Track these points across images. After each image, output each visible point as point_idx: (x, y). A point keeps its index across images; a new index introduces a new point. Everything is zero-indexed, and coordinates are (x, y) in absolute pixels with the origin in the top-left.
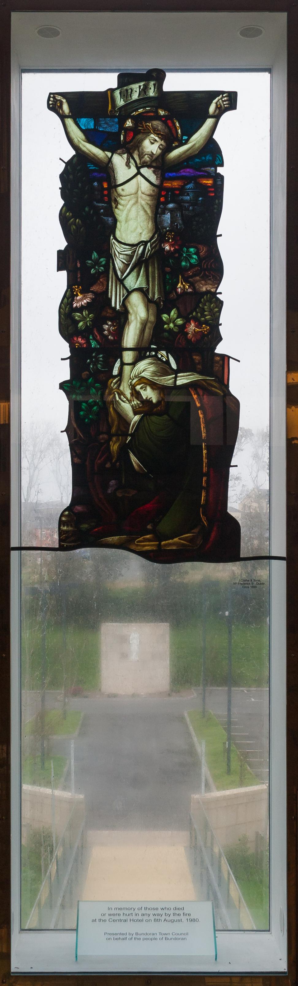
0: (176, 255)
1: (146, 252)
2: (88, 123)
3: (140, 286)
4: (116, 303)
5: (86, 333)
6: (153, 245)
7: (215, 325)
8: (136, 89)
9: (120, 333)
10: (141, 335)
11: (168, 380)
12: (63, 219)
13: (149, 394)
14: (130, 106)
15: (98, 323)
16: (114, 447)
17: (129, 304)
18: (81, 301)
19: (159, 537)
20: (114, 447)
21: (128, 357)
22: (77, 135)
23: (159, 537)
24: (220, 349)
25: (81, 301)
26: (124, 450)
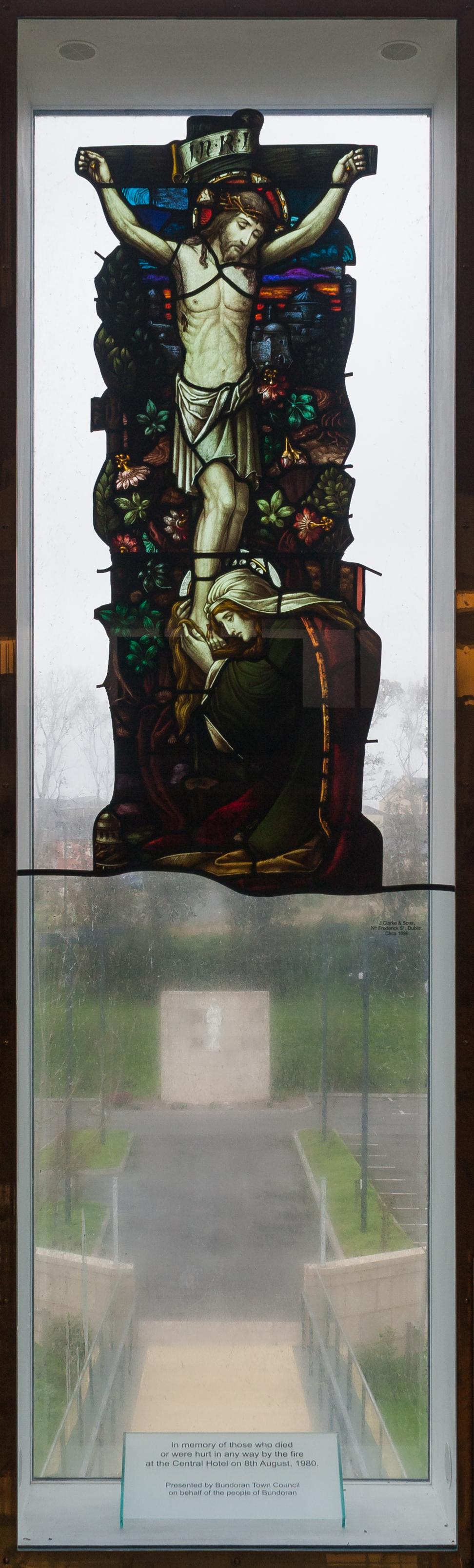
0: (281, 406)
1: (232, 401)
2: (140, 195)
3: (222, 454)
4: (184, 481)
5: (136, 530)
6: (243, 390)
7: (342, 516)
8: (216, 141)
9: (190, 530)
10: (225, 532)
11: (267, 605)
12: (101, 348)
13: (236, 626)
14: (206, 169)
15: (156, 513)
16: (182, 711)
17: (205, 483)
18: (129, 478)
19: (253, 854)
20: (182, 711)
21: (204, 567)
22: (123, 214)
23: (253, 854)
24: (350, 555)
25: (129, 478)
26: (197, 715)
